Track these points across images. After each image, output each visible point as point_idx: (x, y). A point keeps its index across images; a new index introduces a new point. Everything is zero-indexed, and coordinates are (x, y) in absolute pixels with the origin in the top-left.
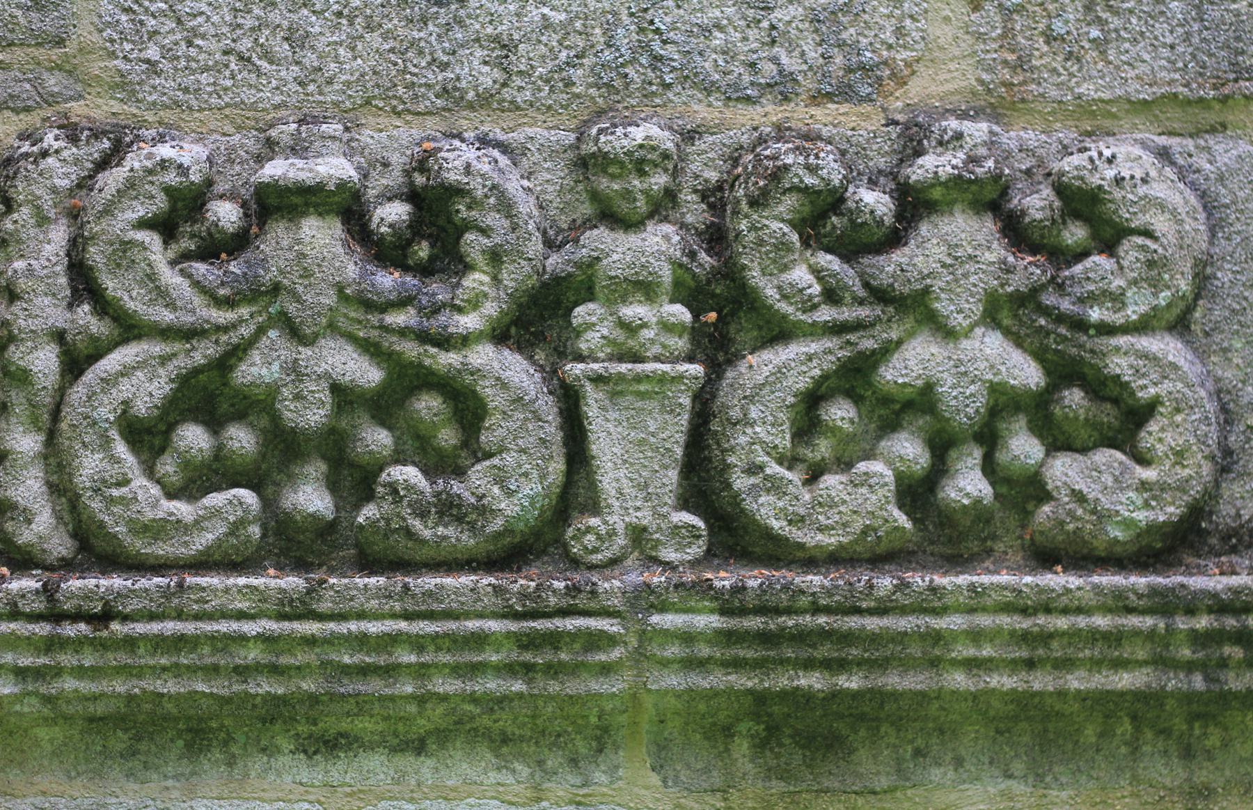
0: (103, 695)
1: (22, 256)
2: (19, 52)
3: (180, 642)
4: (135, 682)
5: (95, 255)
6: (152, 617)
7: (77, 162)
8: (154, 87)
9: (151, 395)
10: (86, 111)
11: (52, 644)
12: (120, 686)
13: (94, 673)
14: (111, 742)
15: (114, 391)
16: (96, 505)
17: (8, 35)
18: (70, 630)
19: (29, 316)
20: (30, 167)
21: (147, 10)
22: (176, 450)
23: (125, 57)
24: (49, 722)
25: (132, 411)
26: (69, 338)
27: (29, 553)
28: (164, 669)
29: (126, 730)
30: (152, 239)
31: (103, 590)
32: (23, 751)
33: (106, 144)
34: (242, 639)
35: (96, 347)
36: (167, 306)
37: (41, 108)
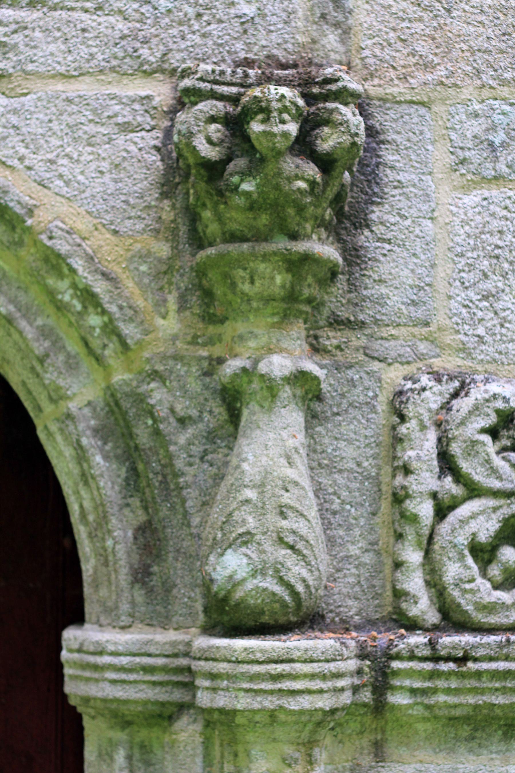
0: (460, 705)
1: (412, 448)
2: (402, 329)
4: (479, 697)
5: (455, 449)
6: (491, 659)
7: (441, 394)
8: (482, 351)
9: (488, 530)
10: (441, 364)
11: (433, 675)
12: (471, 700)
13: (457, 691)
14: (460, 732)
15: (467, 527)
16: (456, 593)
17: (397, 319)
19: (419, 483)
20: (416, 397)
21: (477, 306)
22: (500, 562)
23: (465, 334)
24: (425, 719)
25: (477, 539)
26: (440, 496)
27: (415, 621)
28: (497, 690)
29: (469, 725)
30: (487, 438)
31: (463, 643)
32: (408, 737)
33: (457, 384)
35: (454, 502)
36: (497, 478)
37: (416, 362)
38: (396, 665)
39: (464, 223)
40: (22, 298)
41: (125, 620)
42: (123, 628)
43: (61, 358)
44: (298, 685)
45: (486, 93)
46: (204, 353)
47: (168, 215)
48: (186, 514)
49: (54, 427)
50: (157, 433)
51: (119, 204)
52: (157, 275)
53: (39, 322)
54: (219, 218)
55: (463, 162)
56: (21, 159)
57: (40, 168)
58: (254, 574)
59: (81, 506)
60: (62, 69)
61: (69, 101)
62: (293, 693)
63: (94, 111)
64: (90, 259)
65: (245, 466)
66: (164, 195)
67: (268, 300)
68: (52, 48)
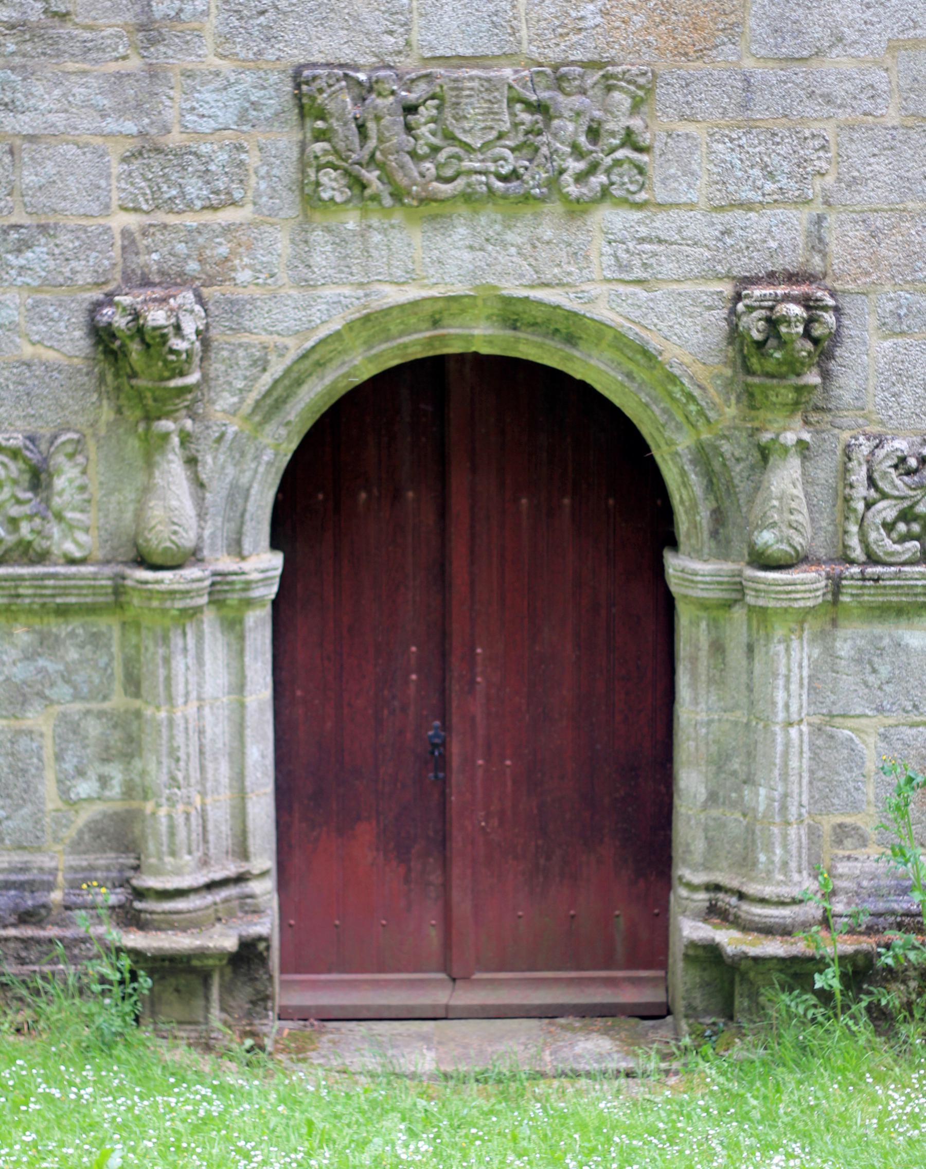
3: (899, 587)
5: (876, 475)
6: (891, 579)
11: (862, 587)
12: (881, 599)
13: (874, 595)
16: (874, 547)
18: (868, 583)
30: (892, 470)
34: (917, 586)
38: (844, 582)
39: (884, 356)
40: (653, 393)
41: (706, 557)
42: (705, 561)
43: (673, 424)
44: (798, 596)
45: (897, 288)
46: (749, 425)
47: (731, 354)
48: (739, 506)
49: (667, 457)
50: (724, 465)
51: (706, 349)
52: (726, 386)
53: (662, 405)
54: (761, 365)
55: (884, 324)
56: (655, 325)
57: (665, 330)
58: (777, 542)
59: (681, 497)
60: (676, 277)
61: (680, 294)
62: (796, 600)
63: (693, 300)
64: (691, 378)
65: (773, 488)
66: (730, 343)
67: (785, 405)
68: (671, 266)
